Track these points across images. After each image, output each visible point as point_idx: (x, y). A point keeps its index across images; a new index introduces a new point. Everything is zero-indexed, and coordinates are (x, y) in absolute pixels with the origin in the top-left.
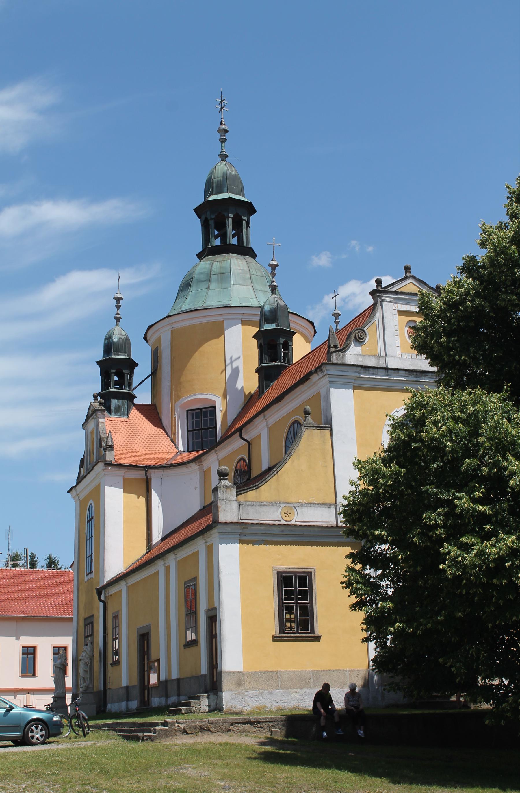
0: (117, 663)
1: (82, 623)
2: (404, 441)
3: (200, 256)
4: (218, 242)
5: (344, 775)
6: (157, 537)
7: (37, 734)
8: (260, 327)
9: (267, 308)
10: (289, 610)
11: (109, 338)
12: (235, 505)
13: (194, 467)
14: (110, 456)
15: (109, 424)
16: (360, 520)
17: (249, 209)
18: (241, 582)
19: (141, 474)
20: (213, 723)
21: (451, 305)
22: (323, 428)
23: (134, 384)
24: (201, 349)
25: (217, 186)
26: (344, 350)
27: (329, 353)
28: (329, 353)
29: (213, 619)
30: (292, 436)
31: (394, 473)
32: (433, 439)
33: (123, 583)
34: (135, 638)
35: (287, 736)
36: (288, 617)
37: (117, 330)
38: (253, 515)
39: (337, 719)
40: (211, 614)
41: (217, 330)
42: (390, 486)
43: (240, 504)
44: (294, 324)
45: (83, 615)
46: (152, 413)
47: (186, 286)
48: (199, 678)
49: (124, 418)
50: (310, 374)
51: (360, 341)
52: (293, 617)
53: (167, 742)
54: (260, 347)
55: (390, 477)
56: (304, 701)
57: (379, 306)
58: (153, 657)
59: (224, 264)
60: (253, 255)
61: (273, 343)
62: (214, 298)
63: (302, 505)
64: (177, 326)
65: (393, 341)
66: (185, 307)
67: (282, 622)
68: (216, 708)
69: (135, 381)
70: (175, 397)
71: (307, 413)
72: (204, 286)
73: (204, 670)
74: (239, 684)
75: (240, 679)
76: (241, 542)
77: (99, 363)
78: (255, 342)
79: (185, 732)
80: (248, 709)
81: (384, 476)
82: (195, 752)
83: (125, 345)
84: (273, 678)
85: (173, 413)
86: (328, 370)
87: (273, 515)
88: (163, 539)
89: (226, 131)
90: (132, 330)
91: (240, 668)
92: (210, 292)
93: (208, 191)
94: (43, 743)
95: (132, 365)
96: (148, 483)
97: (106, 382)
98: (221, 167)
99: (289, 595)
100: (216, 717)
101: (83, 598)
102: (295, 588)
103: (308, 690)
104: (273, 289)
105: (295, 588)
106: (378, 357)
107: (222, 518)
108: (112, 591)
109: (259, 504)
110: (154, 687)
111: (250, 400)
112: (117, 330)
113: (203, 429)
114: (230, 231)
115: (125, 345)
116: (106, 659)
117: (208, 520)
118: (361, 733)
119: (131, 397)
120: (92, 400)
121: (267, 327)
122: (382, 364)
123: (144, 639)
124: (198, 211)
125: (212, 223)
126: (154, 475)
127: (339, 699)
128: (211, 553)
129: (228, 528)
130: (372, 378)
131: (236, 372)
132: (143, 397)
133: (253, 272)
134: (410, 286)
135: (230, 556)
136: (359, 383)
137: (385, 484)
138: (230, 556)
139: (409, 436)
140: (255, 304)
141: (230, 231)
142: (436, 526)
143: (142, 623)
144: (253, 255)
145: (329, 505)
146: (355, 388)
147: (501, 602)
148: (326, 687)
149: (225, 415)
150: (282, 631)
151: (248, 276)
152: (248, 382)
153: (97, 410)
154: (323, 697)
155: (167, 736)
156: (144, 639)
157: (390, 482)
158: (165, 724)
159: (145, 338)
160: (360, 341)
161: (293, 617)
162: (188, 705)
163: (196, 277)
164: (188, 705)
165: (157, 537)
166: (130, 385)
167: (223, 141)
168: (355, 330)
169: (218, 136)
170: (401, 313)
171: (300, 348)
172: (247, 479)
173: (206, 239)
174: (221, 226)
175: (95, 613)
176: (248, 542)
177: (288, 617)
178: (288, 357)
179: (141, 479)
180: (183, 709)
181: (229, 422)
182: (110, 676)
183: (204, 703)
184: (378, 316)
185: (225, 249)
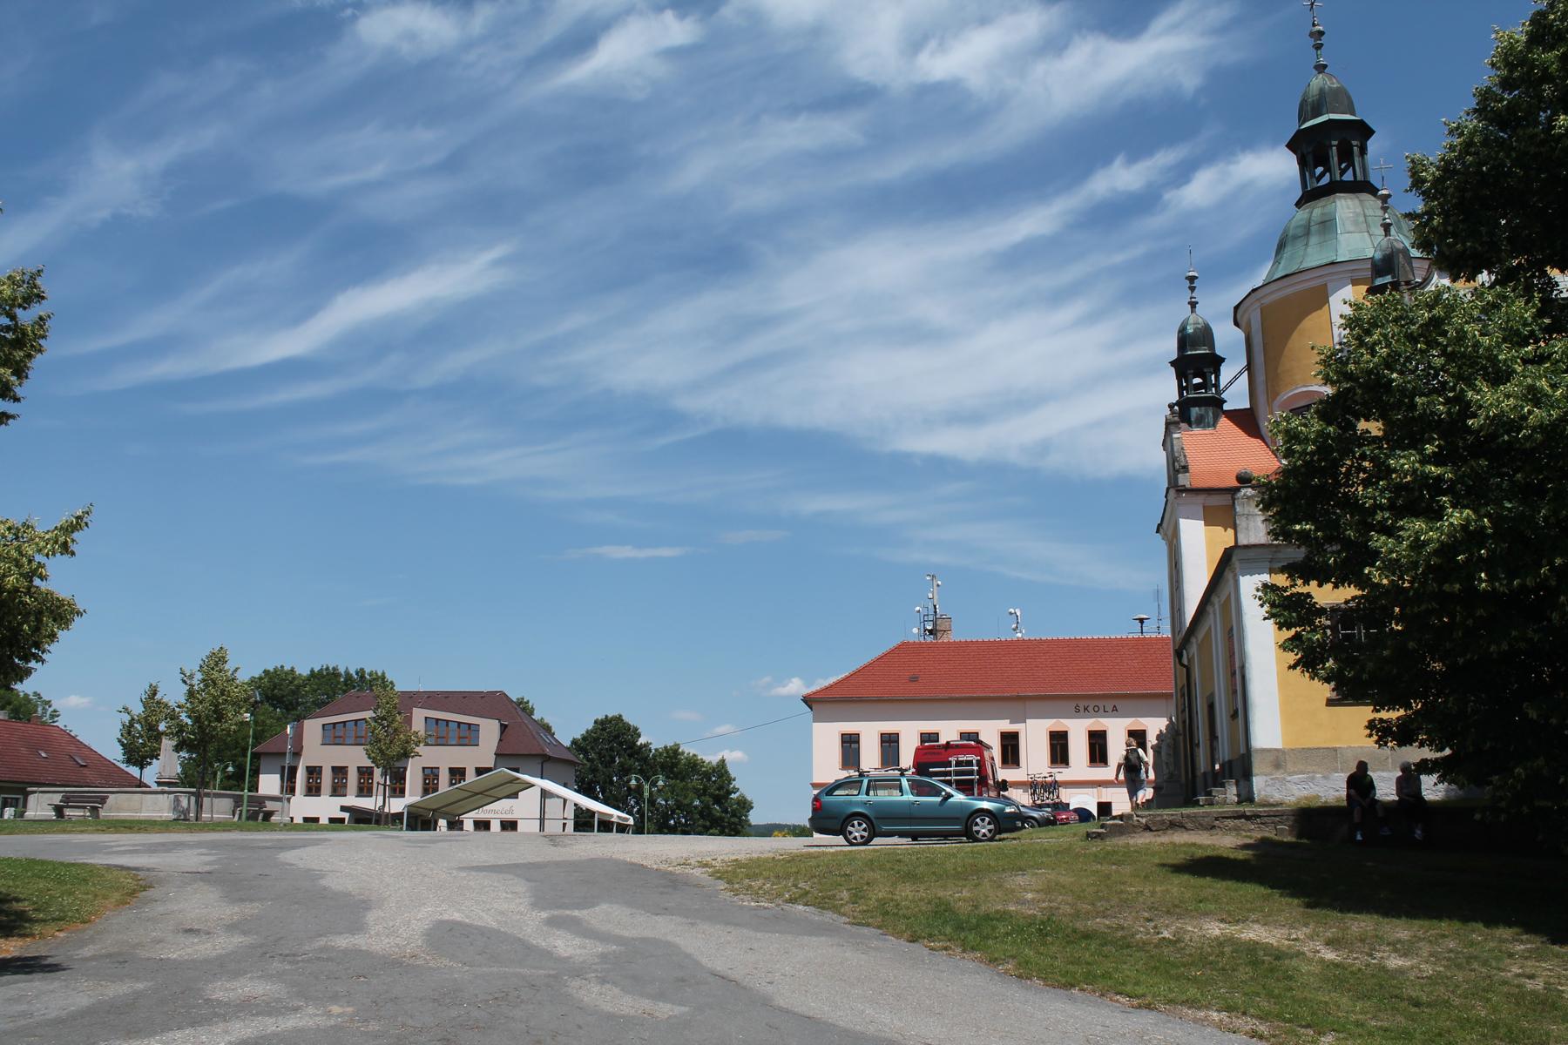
3: (1299, 204)
7: (983, 828)
11: (1182, 330)
15: (1192, 440)
19: (1222, 500)
20: (1188, 816)
21: (1447, 168)
23: (1223, 382)
24: (1301, 326)
25: (1313, 109)
32: (1369, 372)
39: (1380, 814)
42: (1312, 453)
46: (1247, 421)
49: (1210, 430)
59: (1326, 210)
62: (1313, 255)
64: (1266, 301)
68: (1247, 797)
70: (1272, 394)
72: (1300, 244)
74: (1277, 765)
75: (1278, 760)
77: (1173, 363)
79: (1147, 828)
80: (1293, 799)
83: (1205, 335)
89: (1321, 33)
91: (1277, 744)
92: (1309, 250)
94: (991, 839)
95: (1216, 362)
98: (1317, 82)
103: (1384, 774)
118: (1359, 837)
119: (1218, 403)
129: (1251, 553)
132: (1237, 396)
133: (1369, 212)
137: (1304, 452)
142: (1377, 507)
147: (1470, 622)
148: (1362, 766)
151: (1361, 219)
155: (1122, 834)
156: (1211, 707)
157: (1311, 448)
163: (1291, 233)
166: (1217, 385)
167: (1318, 47)
169: (1312, 42)
174: (1324, 160)
183: (1231, 792)
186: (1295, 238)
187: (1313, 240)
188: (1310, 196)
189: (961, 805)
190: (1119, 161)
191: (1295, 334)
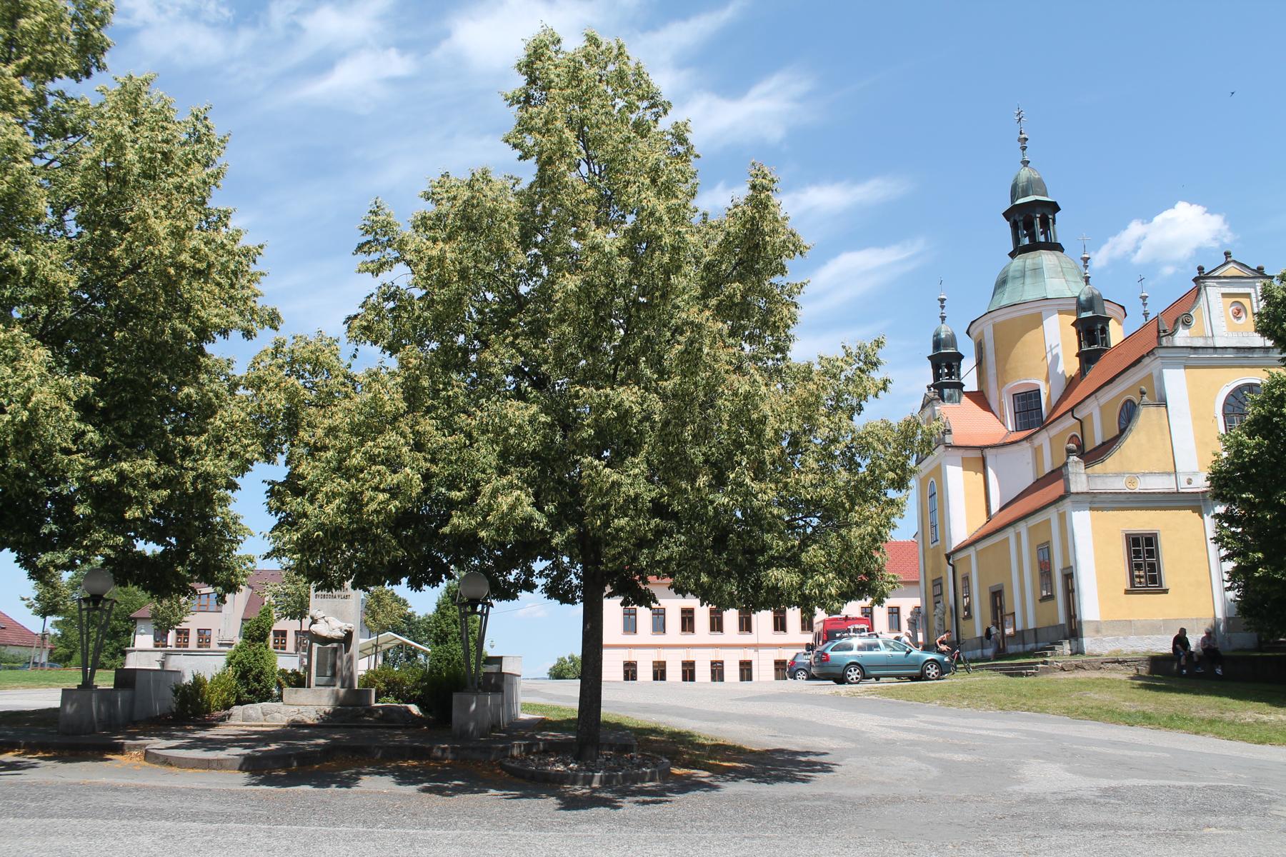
0: (969, 617)
1: (930, 585)
2: (1264, 417)
3: (1012, 255)
4: (1026, 241)
5: (1226, 700)
6: (995, 507)
7: (933, 671)
8: (1078, 314)
9: (1083, 298)
10: (1138, 567)
11: (937, 335)
12: (1084, 477)
13: (1026, 445)
14: (948, 439)
16: (1226, 485)
17: (1054, 207)
18: (1094, 545)
19: (977, 454)
22: (1158, 405)
26: (1172, 334)
27: (1159, 337)
28: (1159, 337)
29: (1069, 576)
30: (1128, 413)
31: (1257, 444)
33: (972, 549)
34: (987, 596)
35: (1151, 672)
36: (1136, 573)
37: (944, 327)
38: (1101, 486)
39: (1196, 659)
40: (1068, 572)
41: (1037, 321)
43: (1088, 477)
44: (1110, 310)
45: (930, 577)
46: (980, 398)
47: (1002, 283)
48: (1057, 627)
50: (1143, 357)
51: (1187, 324)
52: (1142, 573)
53: (1050, 676)
54: (1078, 333)
55: (1254, 448)
56: (1164, 646)
57: (1203, 291)
58: (1007, 610)
60: (1062, 250)
61: (1091, 330)
62: (1030, 292)
63: (1144, 474)
65: (1225, 320)
66: (1005, 302)
67: (1132, 577)
68: (1078, 651)
69: (963, 371)
70: (1001, 383)
71: (1143, 393)
72: (1020, 281)
73: (1062, 620)
74: (1098, 631)
75: (1098, 627)
76: (1091, 509)
78: (1074, 329)
79: (1063, 669)
81: (1248, 448)
82: (1093, 683)
83: (952, 341)
84: (1127, 626)
85: (1000, 398)
86: (1160, 353)
87: (1119, 485)
88: (1001, 510)
90: (955, 327)
93: (1014, 196)
95: (959, 357)
96: (984, 460)
97: (937, 376)
98: (1025, 173)
99: (1137, 554)
100: (1079, 659)
101: (929, 563)
102: (1143, 548)
104: (1087, 280)
105: (1143, 548)
106: (1206, 338)
107: (1073, 489)
108: (960, 556)
109: (1105, 475)
110: (1010, 636)
111: (1072, 383)
112: (944, 327)
113: (1029, 410)
114: (1038, 229)
115: (952, 341)
116: (961, 613)
117: (1055, 489)
118: (1219, 671)
119: (960, 386)
120: (926, 391)
121: (1084, 315)
122: (1210, 344)
123: (997, 596)
124: (1007, 215)
125: (1021, 224)
126: (989, 454)
127: (1195, 640)
128: (1064, 520)
129: (1079, 498)
130: (1205, 357)
131: (1056, 358)
132: (970, 383)
134: (1231, 270)
135: (1082, 521)
136: (1190, 363)
137: (1250, 454)
138: (1082, 521)
139: (1270, 412)
140: (1069, 294)
141: (1038, 229)
143: (994, 582)
144: (1062, 250)
145: (1169, 474)
146: (1186, 367)
148: (1183, 631)
149: (1049, 398)
150: (1132, 585)
152: (1070, 365)
153: (933, 399)
154: (1181, 640)
156: (997, 596)
158: (1045, 663)
159: (968, 333)
160: (1187, 324)
161: (1142, 573)
162: (1052, 649)
163: (1011, 274)
164: (1052, 649)
165: (995, 507)
166: (959, 375)
167: (1024, 149)
168: (1181, 314)
169: (1019, 144)
170: (1224, 295)
171: (1116, 333)
172: (1093, 455)
173: (1016, 240)
174: (1029, 226)
175: (943, 575)
176: (1097, 509)
177: (1136, 573)
178: (1105, 341)
179: (978, 457)
180: (1049, 653)
181: (1053, 404)
182: (961, 628)
183: (1066, 647)
184: (1203, 299)
185: (1035, 246)
186: (1014, 278)
187: (1028, 281)
188: (1018, 251)
189: (917, 658)
190: (720, 187)
191: (1019, 345)
